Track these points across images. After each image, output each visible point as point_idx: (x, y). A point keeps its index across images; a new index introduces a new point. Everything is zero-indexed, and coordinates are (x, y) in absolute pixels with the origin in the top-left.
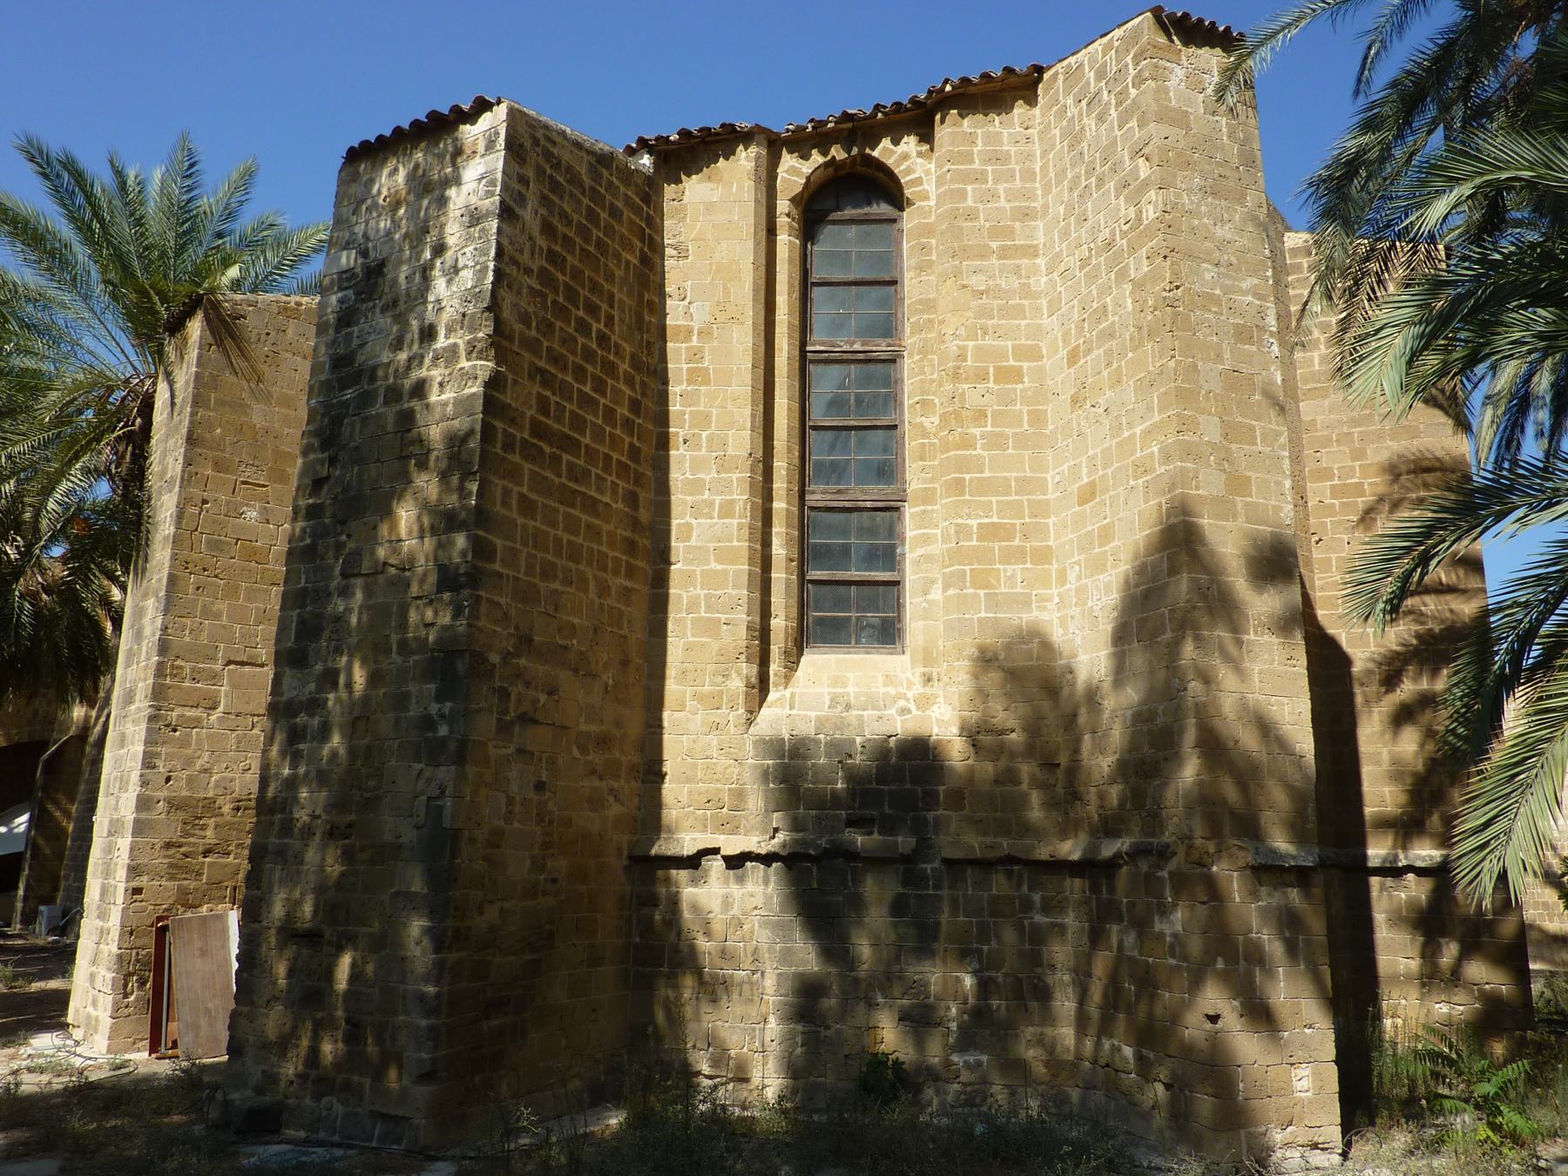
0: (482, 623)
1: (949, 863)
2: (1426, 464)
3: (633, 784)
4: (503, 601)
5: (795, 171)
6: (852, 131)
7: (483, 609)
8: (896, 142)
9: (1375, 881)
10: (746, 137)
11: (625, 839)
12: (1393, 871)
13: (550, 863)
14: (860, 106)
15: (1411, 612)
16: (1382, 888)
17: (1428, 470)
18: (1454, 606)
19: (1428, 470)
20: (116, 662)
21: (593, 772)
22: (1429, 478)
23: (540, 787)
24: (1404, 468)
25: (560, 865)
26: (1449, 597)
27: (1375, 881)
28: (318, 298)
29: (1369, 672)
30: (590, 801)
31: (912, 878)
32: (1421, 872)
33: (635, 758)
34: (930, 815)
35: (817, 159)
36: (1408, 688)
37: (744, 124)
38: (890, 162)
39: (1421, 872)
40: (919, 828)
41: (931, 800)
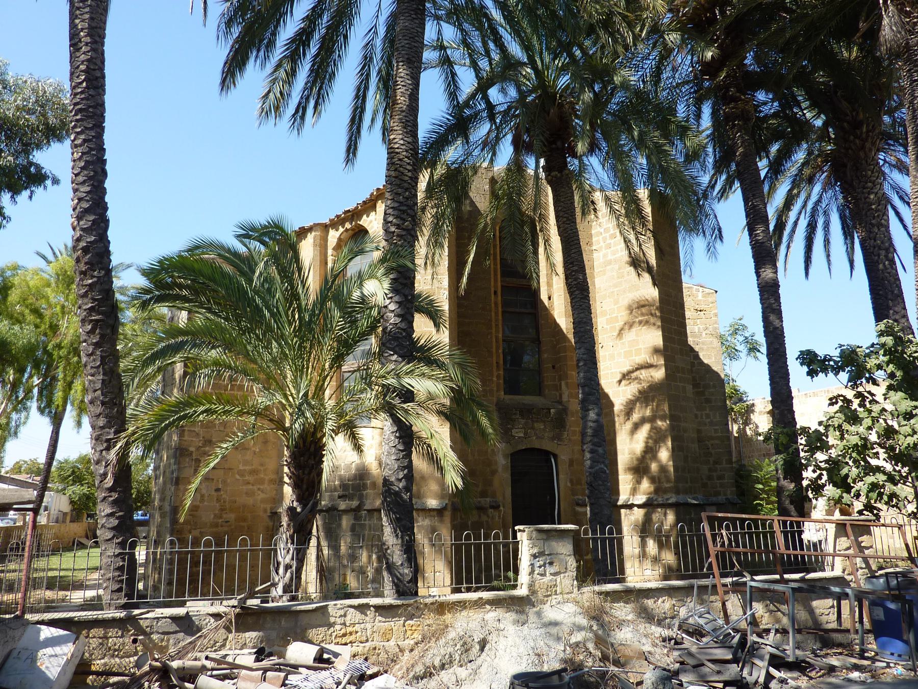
0: (186, 438)
1: (368, 511)
2: (642, 303)
3: (272, 486)
4: (196, 430)
5: (334, 236)
6: (353, 216)
7: (186, 433)
8: (368, 216)
9: (623, 511)
10: (310, 229)
11: (268, 507)
12: (630, 507)
13: (224, 516)
14: (351, 206)
15: (636, 378)
16: (626, 515)
17: (643, 306)
18: (652, 374)
19: (643, 306)
20: (900, 295)
21: (249, 483)
22: (644, 310)
23: (218, 490)
24: (635, 306)
25: (231, 516)
26: (651, 370)
27: (623, 511)
28: (435, 210)
29: (621, 411)
30: (246, 493)
31: (357, 518)
32: (639, 506)
33: (273, 476)
34: (365, 493)
35: (341, 230)
36: (636, 416)
37: (307, 225)
38: (365, 225)
39: (639, 506)
40: (361, 498)
41: (365, 487)
